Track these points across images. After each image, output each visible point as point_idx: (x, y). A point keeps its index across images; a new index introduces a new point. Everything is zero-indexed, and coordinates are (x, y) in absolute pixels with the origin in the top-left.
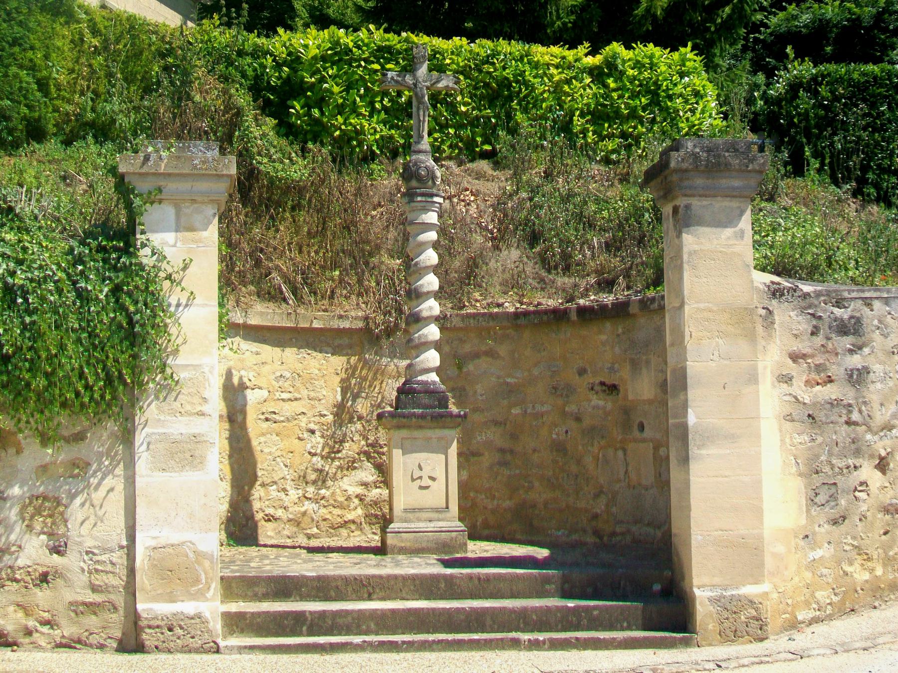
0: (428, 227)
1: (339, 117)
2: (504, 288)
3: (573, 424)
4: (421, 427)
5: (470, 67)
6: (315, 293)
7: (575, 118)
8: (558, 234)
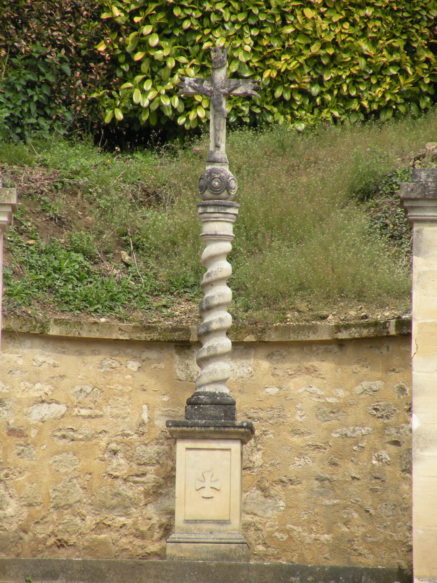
0: (217, 237)
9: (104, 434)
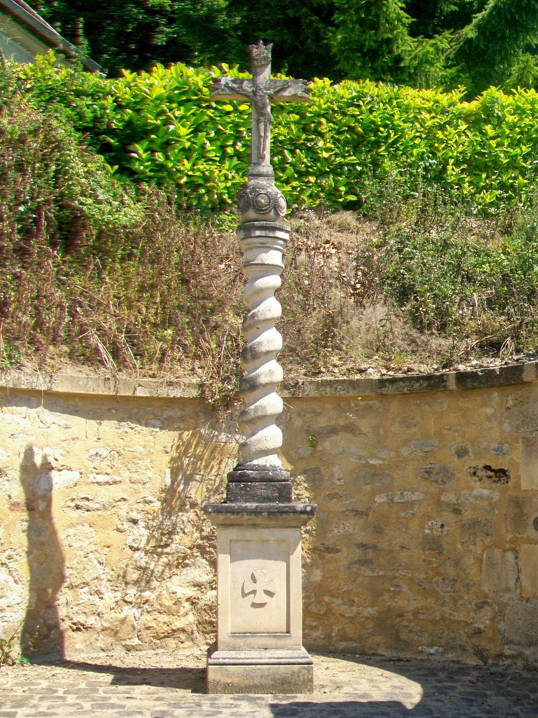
1: (186, 161)
2: (368, 351)
3: (449, 517)
4: (255, 526)
5: (333, 110)
6: (142, 356)
7: (450, 167)
8: (431, 289)
9: (123, 502)
